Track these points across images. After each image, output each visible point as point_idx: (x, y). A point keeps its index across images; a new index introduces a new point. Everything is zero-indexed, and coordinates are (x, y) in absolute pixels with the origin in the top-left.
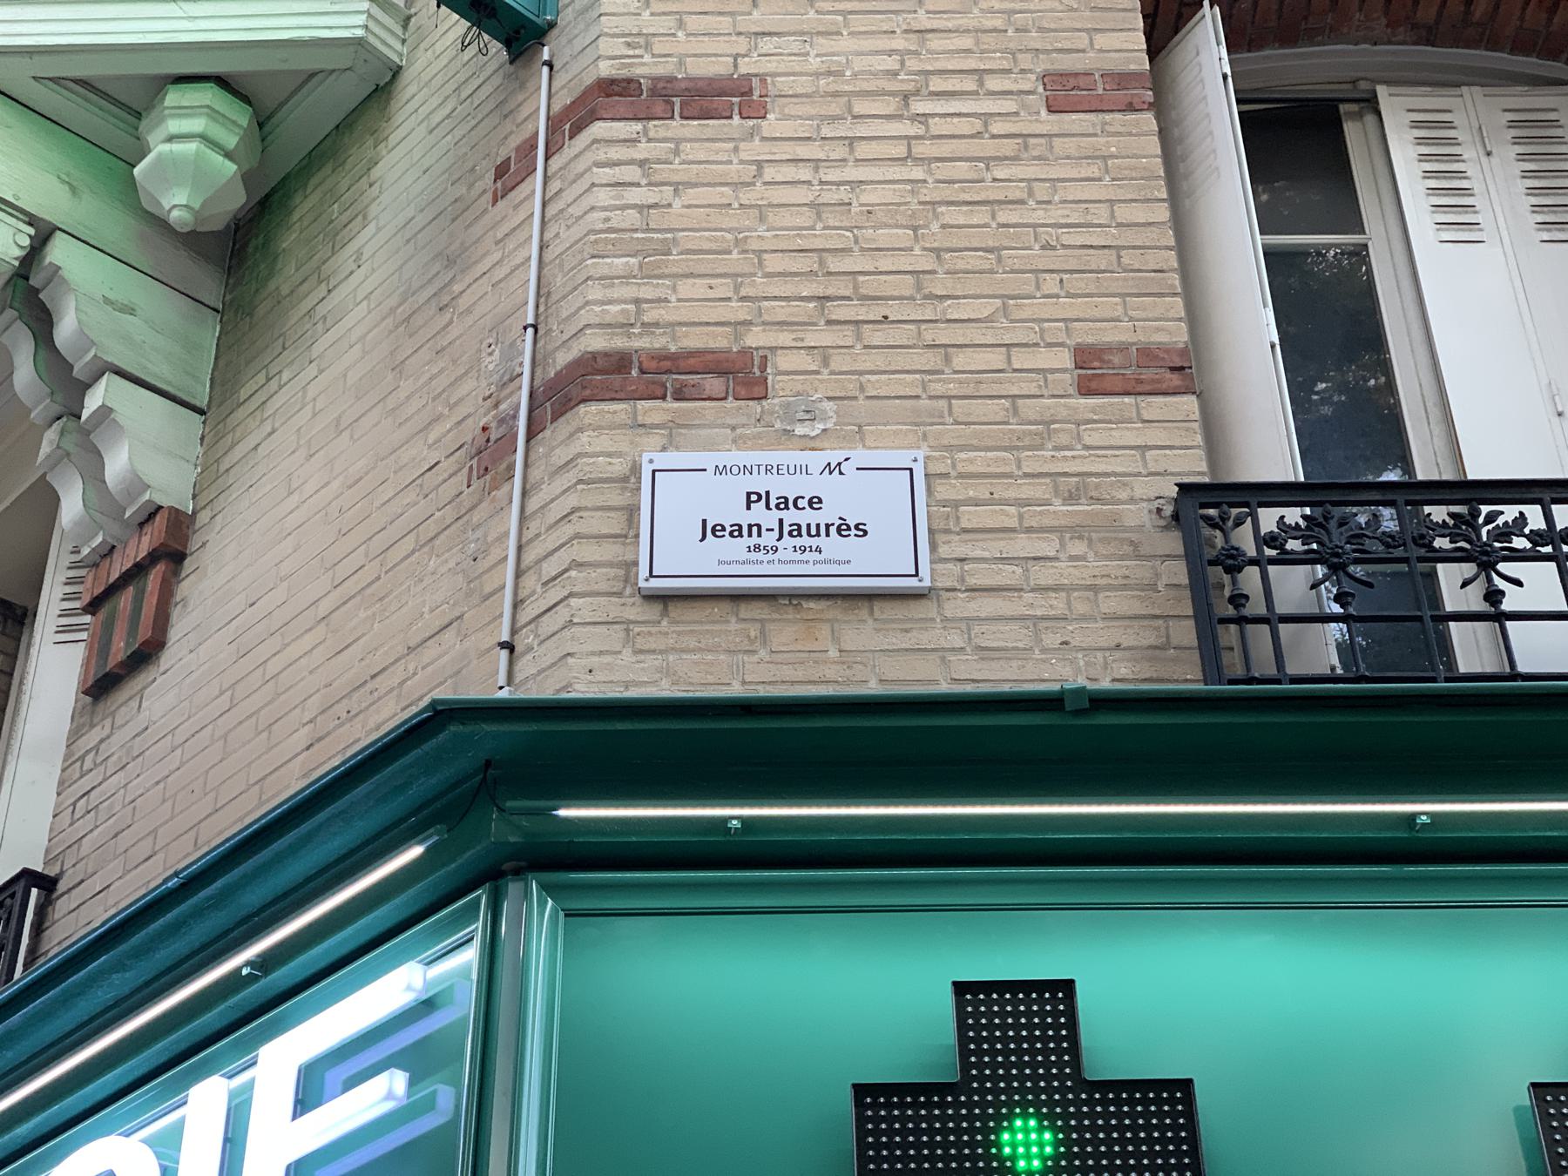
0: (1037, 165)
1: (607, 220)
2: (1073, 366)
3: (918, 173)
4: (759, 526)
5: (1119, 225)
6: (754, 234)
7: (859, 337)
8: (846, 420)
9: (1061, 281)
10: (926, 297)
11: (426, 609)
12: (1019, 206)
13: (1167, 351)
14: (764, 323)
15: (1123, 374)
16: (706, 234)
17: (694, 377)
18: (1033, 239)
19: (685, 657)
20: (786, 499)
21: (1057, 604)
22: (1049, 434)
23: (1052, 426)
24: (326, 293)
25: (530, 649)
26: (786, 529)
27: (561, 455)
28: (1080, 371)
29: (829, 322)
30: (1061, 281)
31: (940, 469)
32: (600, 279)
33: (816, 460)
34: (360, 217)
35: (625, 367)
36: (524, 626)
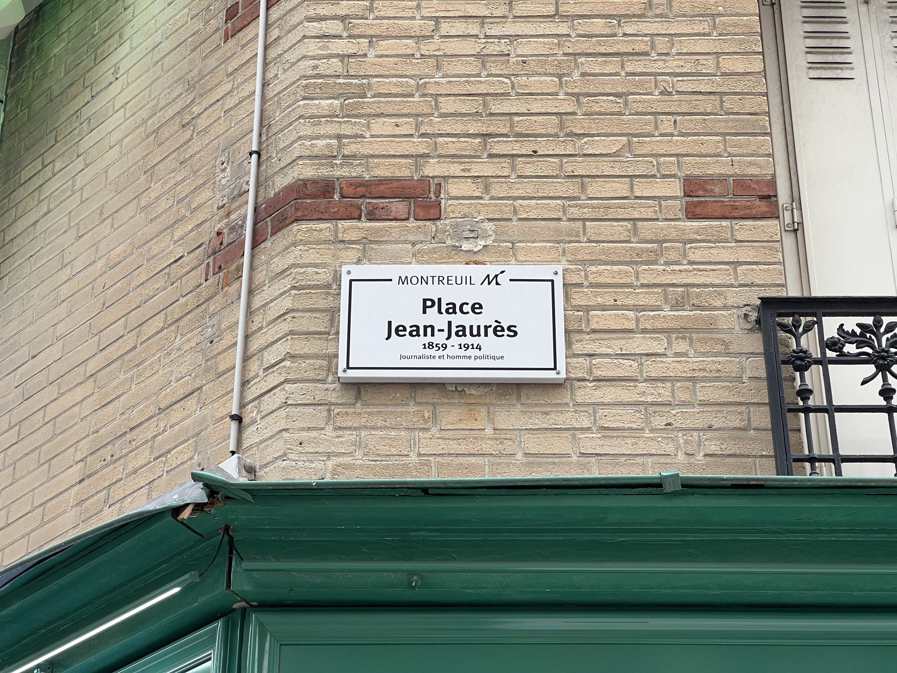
0: (659, 22)
1: (316, 67)
2: (683, 194)
3: (563, 28)
4: (432, 327)
5: (724, 74)
6: (432, 80)
7: (513, 168)
8: (503, 238)
9: (675, 122)
10: (567, 135)
11: (173, 378)
12: (643, 58)
13: (758, 182)
14: (439, 156)
15: (722, 202)
16: (394, 80)
17: (383, 201)
18: (653, 86)
19: (373, 433)
20: (454, 305)
21: (664, 392)
22: (662, 251)
23: (664, 245)
24: (90, 98)
25: (254, 422)
26: (454, 330)
27: (279, 263)
28: (688, 199)
29: (491, 156)
30: (675, 122)
31: (575, 279)
32: (309, 117)
33: (478, 272)
34: (117, 36)
35: (329, 192)
36: (250, 402)
